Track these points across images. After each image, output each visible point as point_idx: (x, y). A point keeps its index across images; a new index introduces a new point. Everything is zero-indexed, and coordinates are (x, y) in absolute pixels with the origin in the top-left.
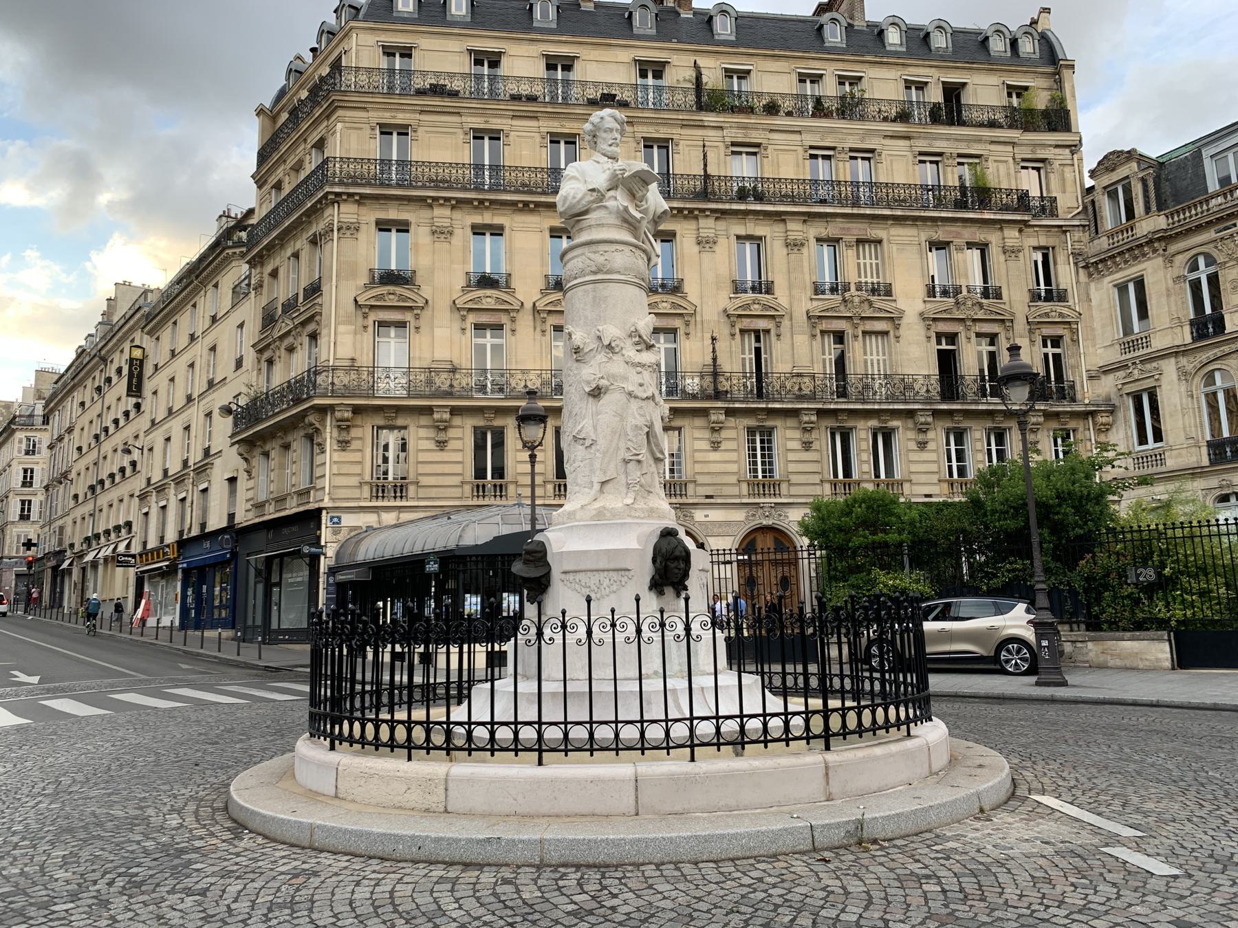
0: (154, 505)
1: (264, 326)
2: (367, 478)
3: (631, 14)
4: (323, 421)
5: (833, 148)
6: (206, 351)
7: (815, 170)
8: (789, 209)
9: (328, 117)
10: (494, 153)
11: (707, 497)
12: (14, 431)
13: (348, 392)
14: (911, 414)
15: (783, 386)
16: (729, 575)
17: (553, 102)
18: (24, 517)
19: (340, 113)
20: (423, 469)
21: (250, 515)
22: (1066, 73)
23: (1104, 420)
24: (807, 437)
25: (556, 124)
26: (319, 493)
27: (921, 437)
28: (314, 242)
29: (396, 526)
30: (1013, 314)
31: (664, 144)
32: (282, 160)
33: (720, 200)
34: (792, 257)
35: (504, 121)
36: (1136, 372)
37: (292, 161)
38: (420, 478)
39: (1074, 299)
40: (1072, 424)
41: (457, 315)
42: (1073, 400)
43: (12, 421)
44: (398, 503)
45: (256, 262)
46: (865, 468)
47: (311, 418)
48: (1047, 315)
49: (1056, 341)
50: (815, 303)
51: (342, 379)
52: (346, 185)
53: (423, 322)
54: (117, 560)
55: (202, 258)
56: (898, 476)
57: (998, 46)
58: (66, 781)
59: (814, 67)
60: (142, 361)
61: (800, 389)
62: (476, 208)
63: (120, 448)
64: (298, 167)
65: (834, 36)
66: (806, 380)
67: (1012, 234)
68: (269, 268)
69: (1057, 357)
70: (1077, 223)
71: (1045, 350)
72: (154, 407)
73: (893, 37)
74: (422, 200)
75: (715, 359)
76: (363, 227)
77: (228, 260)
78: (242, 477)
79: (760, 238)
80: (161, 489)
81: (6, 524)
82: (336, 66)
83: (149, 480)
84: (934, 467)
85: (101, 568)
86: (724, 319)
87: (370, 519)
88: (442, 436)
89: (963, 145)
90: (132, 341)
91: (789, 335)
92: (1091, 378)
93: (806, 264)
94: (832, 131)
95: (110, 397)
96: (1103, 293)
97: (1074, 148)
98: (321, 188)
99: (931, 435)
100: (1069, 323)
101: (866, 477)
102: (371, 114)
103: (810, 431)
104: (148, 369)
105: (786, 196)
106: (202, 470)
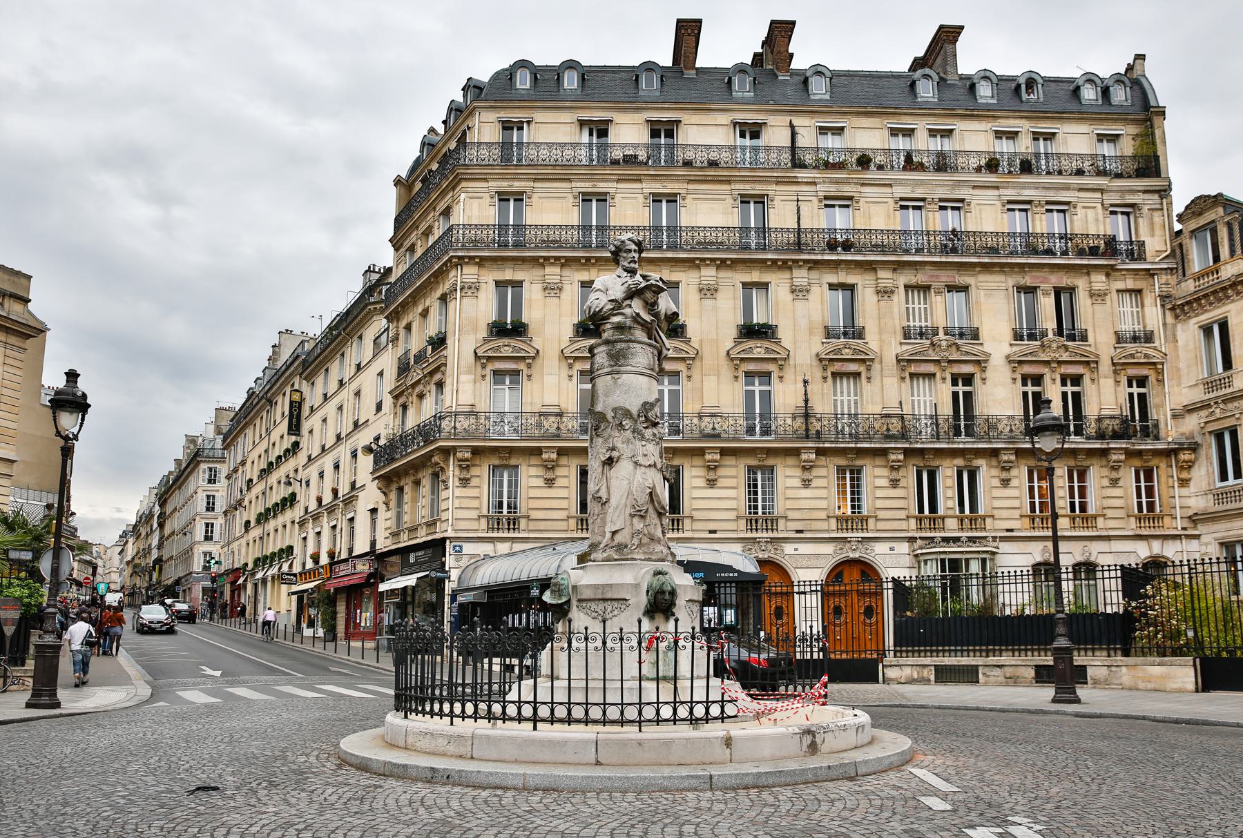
0: (311, 531)
1: (399, 375)
2: (485, 512)
3: (730, 79)
4: (446, 460)
5: (923, 200)
6: (352, 395)
7: (905, 220)
8: (878, 258)
9: (453, 189)
10: (602, 214)
11: (798, 532)
12: (198, 463)
13: (468, 434)
14: (995, 453)
15: (871, 427)
16: (814, 605)
17: (657, 166)
18: (208, 538)
19: (464, 184)
20: (533, 504)
21: (389, 542)
22: (1156, 120)
23: (1187, 457)
24: (894, 475)
25: (658, 185)
26: (444, 525)
27: (1004, 475)
28: (444, 299)
29: (509, 555)
30: (1098, 356)
31: (760, 200)
32: (416, 226)
33: (812, 251)
34: (882, 303)
35: (610, 185)
36: (1218, 411)
37: (423, 227)
38: (531, 513)
39: (1160, 341)
40: (1153, 462)
41: (564, 365)
42: (1157, 438)
43: (197, 454)
44: (511, 535)
45: (393, 317)
46: (950, 504)
47: (436, 459)
48: (1132, 356)
49: (1142, 382)
50: (905, 348)
51: (463, 423)
52: (468, 249)
53: (535, 372)
54: (281, 578)
55: (348, 312)
56: (981, 511)
57: (1089, 94)
58: (237, 736)
59: (906, 122)
60: (300, 404)
61: (888, 430)
62: (583, 265)
63: (284, 480)
64: (428, 232)
65: (927, 91)
66: (894, 420)
67: (1099, 280)
68: (403, 323)
69: (1142, 397)
70: (1165, 266)
71: (1131, 390)
72: (310, 445)
73: (985, 91)
74: (536, 259)
75: (806, 401)
76: (483, 286)
77: (369, 317)
78: (382, 508)
79: (853, 286)
80: (316, 517)
81: (194, 543)
82: (462, 141)
83: (306, 509)
84: (1016, 503)
85: (269, 584)
86: (815, 363)
87: (486, 548)
88: (550, 475)
89: (1051, 193)
90: (293, 385)
91: (879, 377)
92: (1174, 417)
93: (896, 310)
94: (921, 183)
95: (275, 436)
96: (1189, 332)
97: (1164, 192)
98: (447, 252)
99: (1014, 472)
100: (1154, 364)
101: (950, 512)
102: (490, 184)
103: (897, 469)
104: (306, 411)
105: (876, 246)
106: (350, 501)
